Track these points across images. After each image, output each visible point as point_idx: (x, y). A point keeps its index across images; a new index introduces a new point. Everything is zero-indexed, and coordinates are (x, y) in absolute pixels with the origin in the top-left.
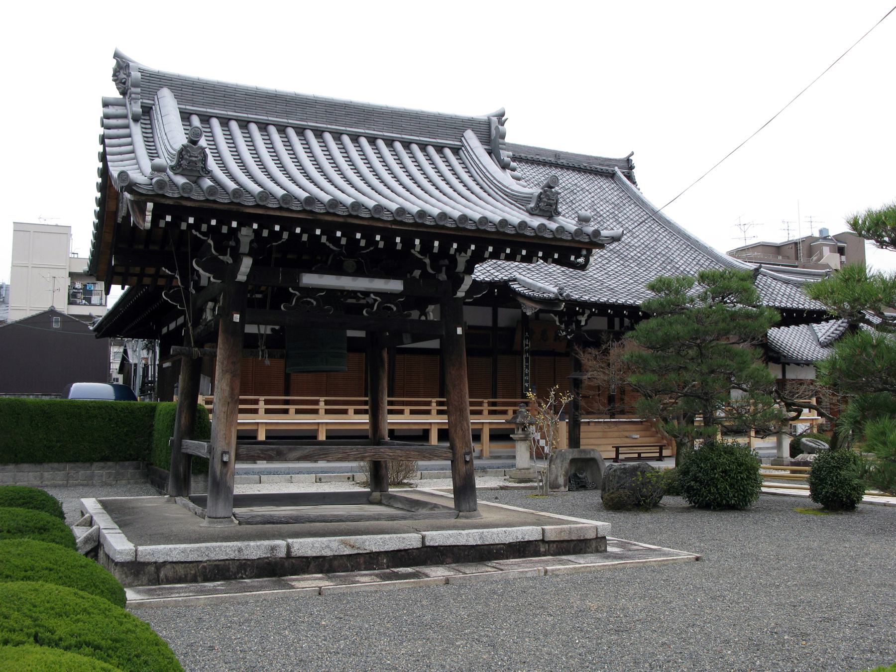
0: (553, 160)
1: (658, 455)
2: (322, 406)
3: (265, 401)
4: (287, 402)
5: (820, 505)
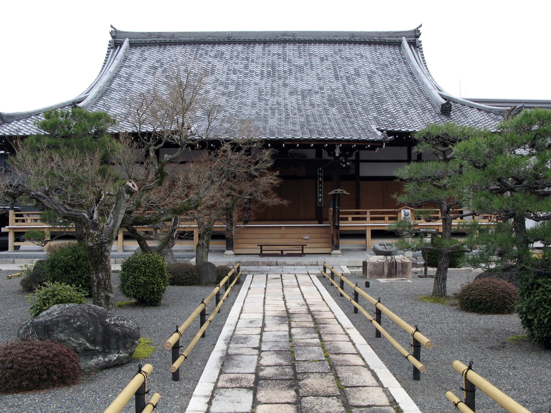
0: (347, 38)
1: (300, 252)
2: (368, 216)
3: (370, 212)
4: (384, 213)
5: (134, 301)
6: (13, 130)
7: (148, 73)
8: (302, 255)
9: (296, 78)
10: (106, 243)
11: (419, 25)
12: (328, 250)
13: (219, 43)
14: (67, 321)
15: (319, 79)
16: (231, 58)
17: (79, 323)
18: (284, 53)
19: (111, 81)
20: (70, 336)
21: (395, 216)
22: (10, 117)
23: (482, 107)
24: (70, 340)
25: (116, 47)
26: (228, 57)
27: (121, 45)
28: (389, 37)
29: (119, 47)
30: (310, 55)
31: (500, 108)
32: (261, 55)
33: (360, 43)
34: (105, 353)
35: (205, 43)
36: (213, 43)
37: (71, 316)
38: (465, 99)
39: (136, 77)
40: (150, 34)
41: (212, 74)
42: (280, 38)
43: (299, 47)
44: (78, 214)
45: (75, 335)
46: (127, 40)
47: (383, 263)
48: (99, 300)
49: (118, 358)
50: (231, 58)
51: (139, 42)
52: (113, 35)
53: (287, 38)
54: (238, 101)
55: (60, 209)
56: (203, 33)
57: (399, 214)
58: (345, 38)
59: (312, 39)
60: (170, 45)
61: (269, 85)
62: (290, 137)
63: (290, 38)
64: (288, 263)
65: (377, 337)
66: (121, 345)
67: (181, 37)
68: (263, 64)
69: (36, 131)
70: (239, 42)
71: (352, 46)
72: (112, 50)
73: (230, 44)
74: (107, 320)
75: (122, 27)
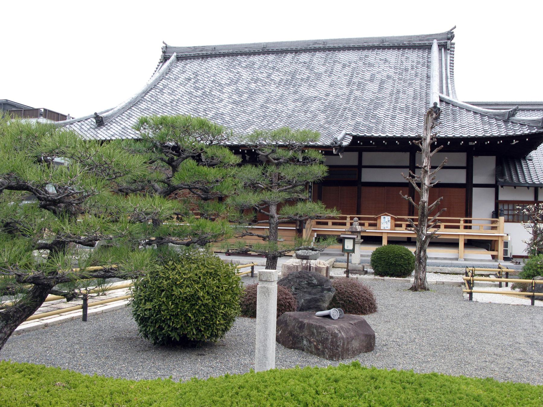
0: (376, 44)
11: (453, 26)
21: (375, 222)
23: (479, 110)
28: (420, 40)
31: (498, 111)
33: (389, 48)
35: (242, 54)
38: (466, 102)
42: (310, 46)
46: (175, 54)
47: (297, 266)
56: (241, 45)
57: (378, 220)
58: (374, 44)
59: (341, 46)
64: (241, 262)
67: (221, 50)
70: (273, 52)
71: (380, 52)
75: (170, 44)
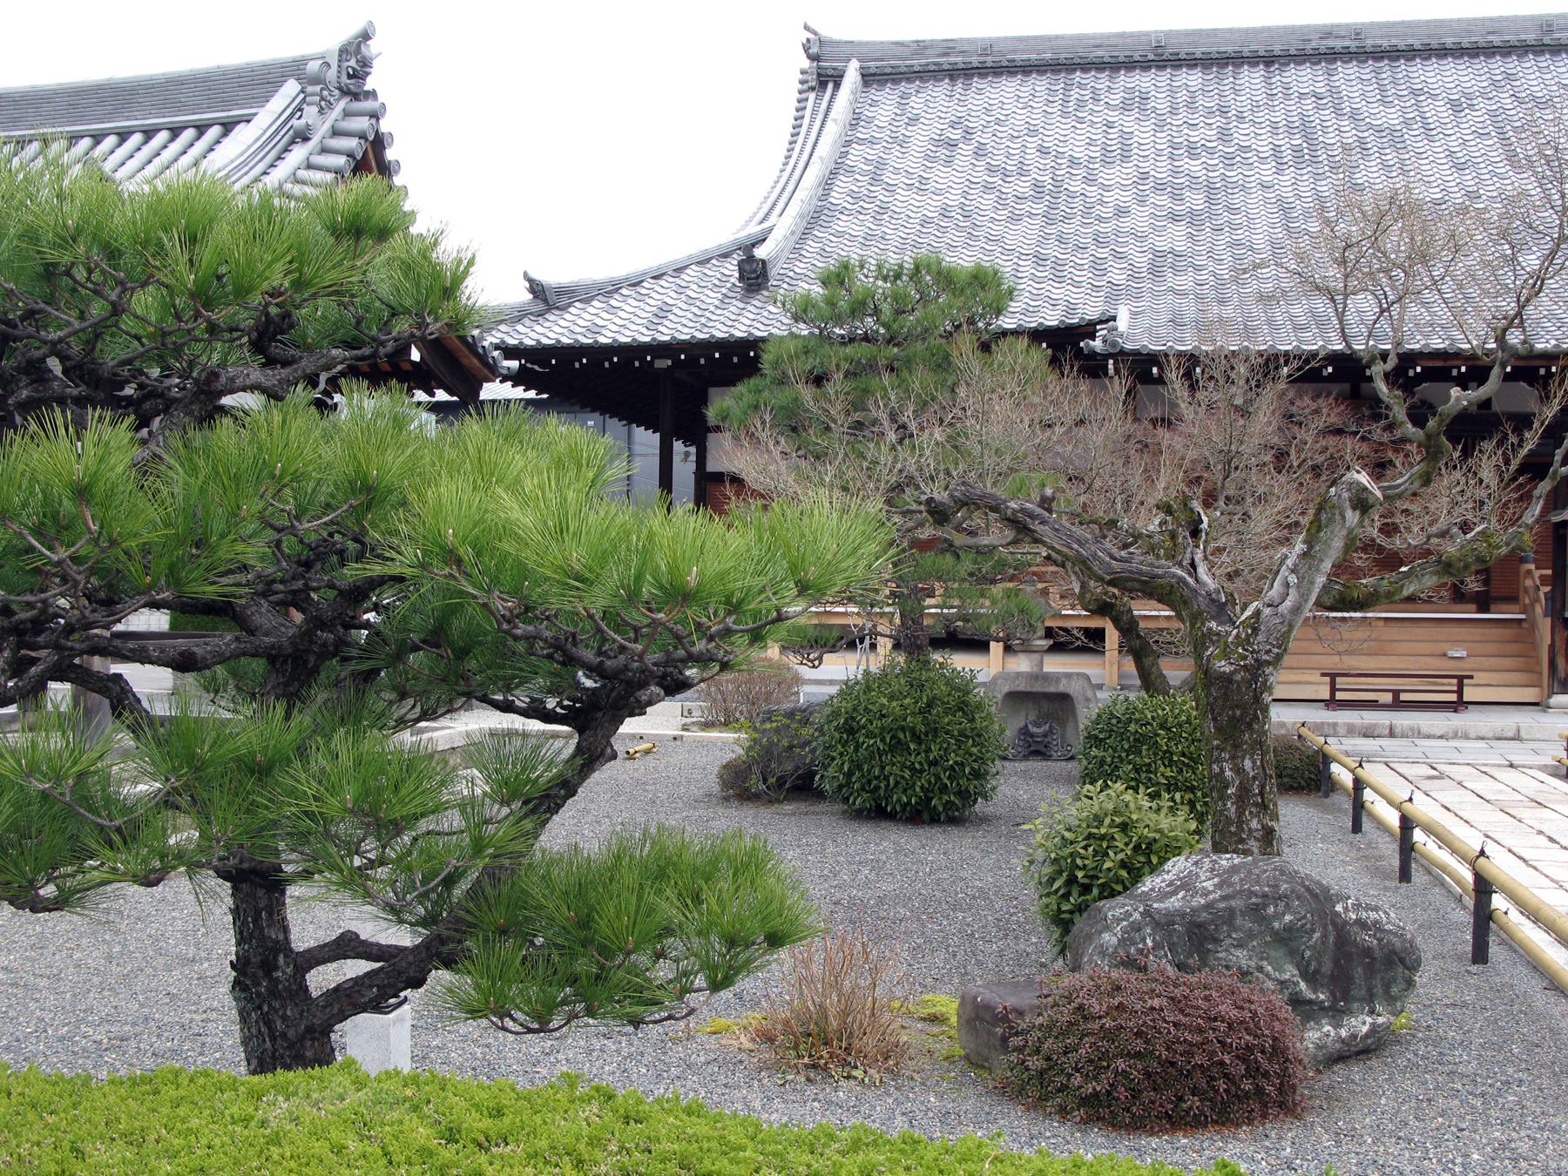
0: (1530, 37)
1: (1454, 697)
6: (578, 330)
7: (933, 159)
8: (1459, 705)
9: (1385, 166)
10: (1268, 663)
12: (1529, 694)
13: (1130, 65)
14: (1256, 912)
15: (1460, 168)
16: (1173, 111)
17: (1288, 918)
18: (1333, 91)
19: (827, 184)
20: (1262, 959)
22: (567, 293)
24: (1260, 969)
25: (823, 85)
26: (1163, 107)
27: (837, 79)
29: (830, 86)
30: (1415, 93)
32: (1261, 97)
34: (1336, 1013)
35: (1087, 66)
36: (1113, 66)
37: (1265, 896)
39: (896, 171)
40: (921, 47)
41: (1125, 158)
42: (1314, 44)
43: (1377, 72)
44: (1160, 571)
45: (1272, 953)
48: (1242, 841)
49: (1374, 1028)
50: (1173, 111)
51: (888, 70)
52: (814, 50)
53: (1338, 44)
54: (1225, 237)
55: (1095, 555)
58: (1523, 37)
59: (1417, 45)
60: (982, 76)
61: (1305, 188)
62: (1437, 343)
63: (1347, 43)
64: (1425, 730)
65: (1475, 961)
66: (1379, 990)
67: (1014, 52)
68: (1274, 126)
69: (644, 331)
70: (1192, 62)
71: (1545, 60)
72: (812, 96)
73: (1162, 68)
74: (1339, 908)
